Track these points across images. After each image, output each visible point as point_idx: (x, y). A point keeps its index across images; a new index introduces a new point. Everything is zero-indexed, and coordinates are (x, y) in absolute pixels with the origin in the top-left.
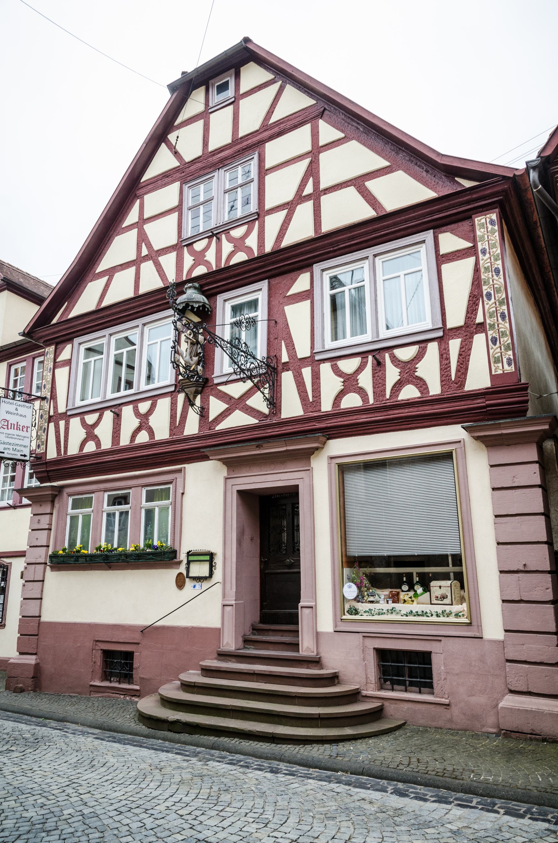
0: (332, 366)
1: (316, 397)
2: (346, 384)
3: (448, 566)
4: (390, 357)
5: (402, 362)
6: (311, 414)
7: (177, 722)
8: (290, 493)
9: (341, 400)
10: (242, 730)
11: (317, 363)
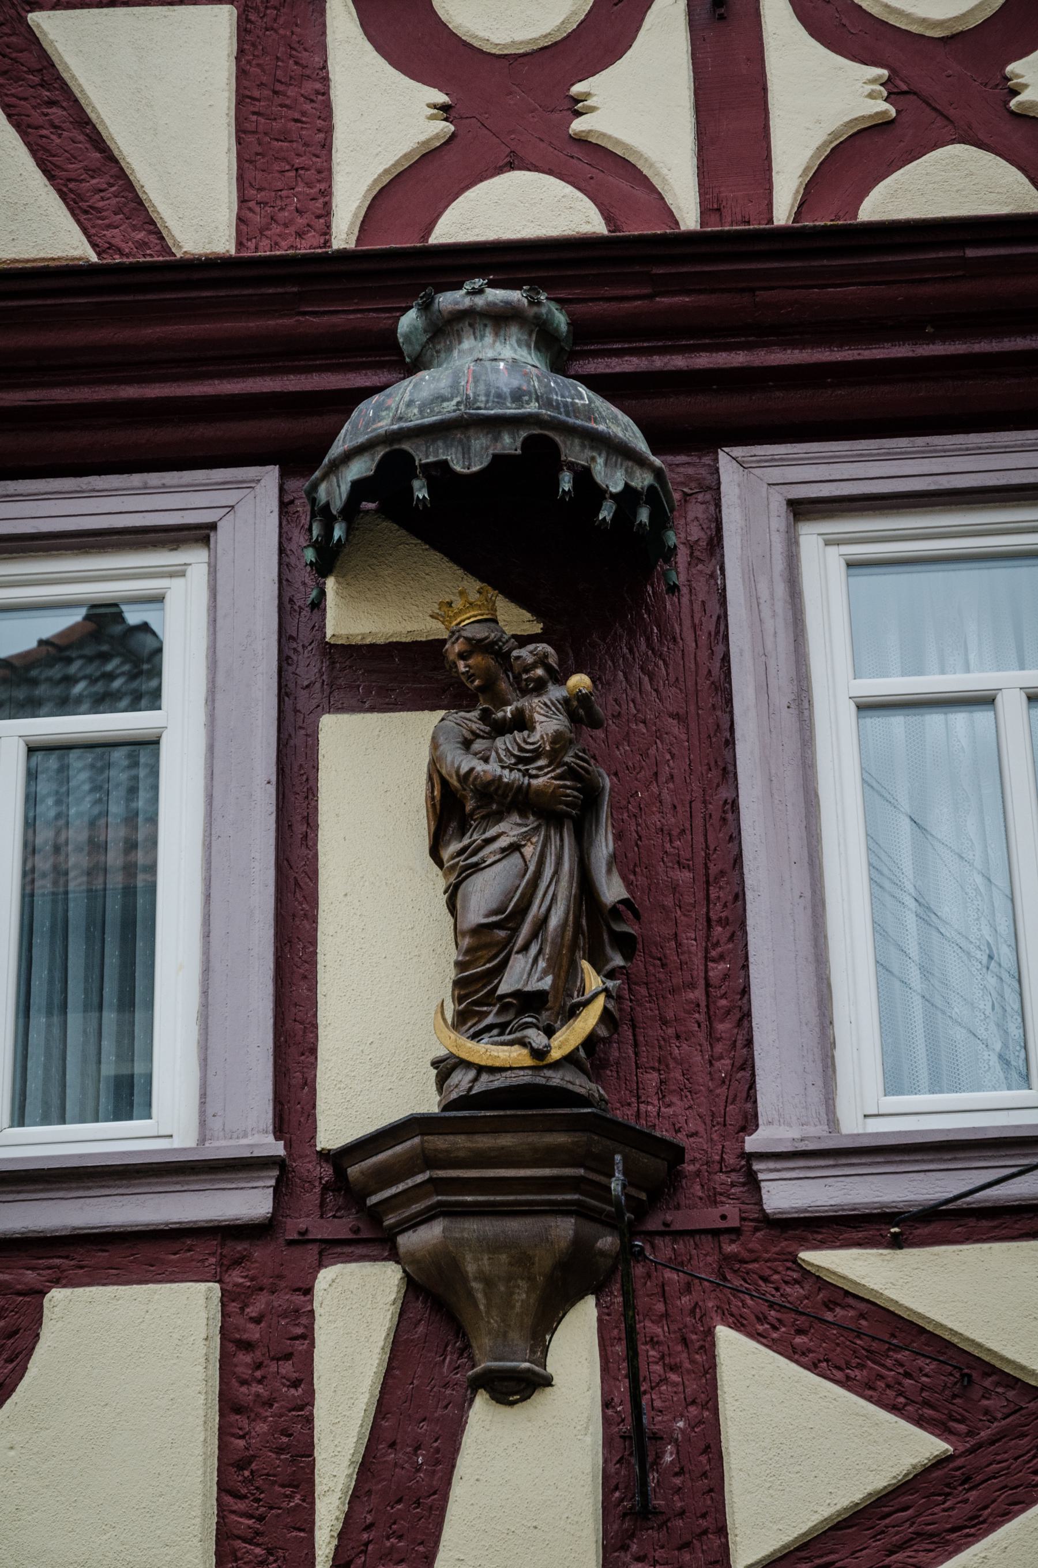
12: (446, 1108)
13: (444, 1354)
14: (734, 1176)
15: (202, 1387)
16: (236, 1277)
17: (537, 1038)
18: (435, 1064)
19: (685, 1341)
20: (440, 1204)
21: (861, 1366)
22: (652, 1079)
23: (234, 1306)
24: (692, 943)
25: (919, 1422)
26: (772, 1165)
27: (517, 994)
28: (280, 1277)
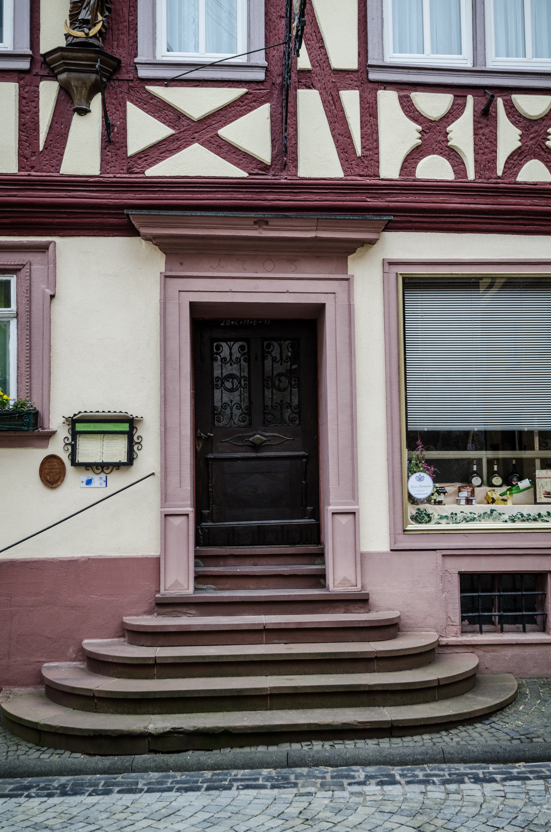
0: (400, 98)
1: (369, 150)
2: (426, 136)
3: (533, 449)
4: (505, 105)
5: (525, 118)
6: (359, 178)
7: (174, 732)
8: (258, 320)
9: (417, 163)
10: (328, 725)
11: (371, 85)
12: (67, 45)
13: (68, 103)
14: (132, 68)
15: (14, 107)
16: (22, 82)
17: (86, 30)
18: (65, 35)
19: (120, 104)
20: (66, 68)
21: (157, 113)
22: (115, 43)
23: (21, 89)
24: (126, 11)
25: (169, 126)
26: (140, 66)
27: (83, 19)
28: (32, 83)
